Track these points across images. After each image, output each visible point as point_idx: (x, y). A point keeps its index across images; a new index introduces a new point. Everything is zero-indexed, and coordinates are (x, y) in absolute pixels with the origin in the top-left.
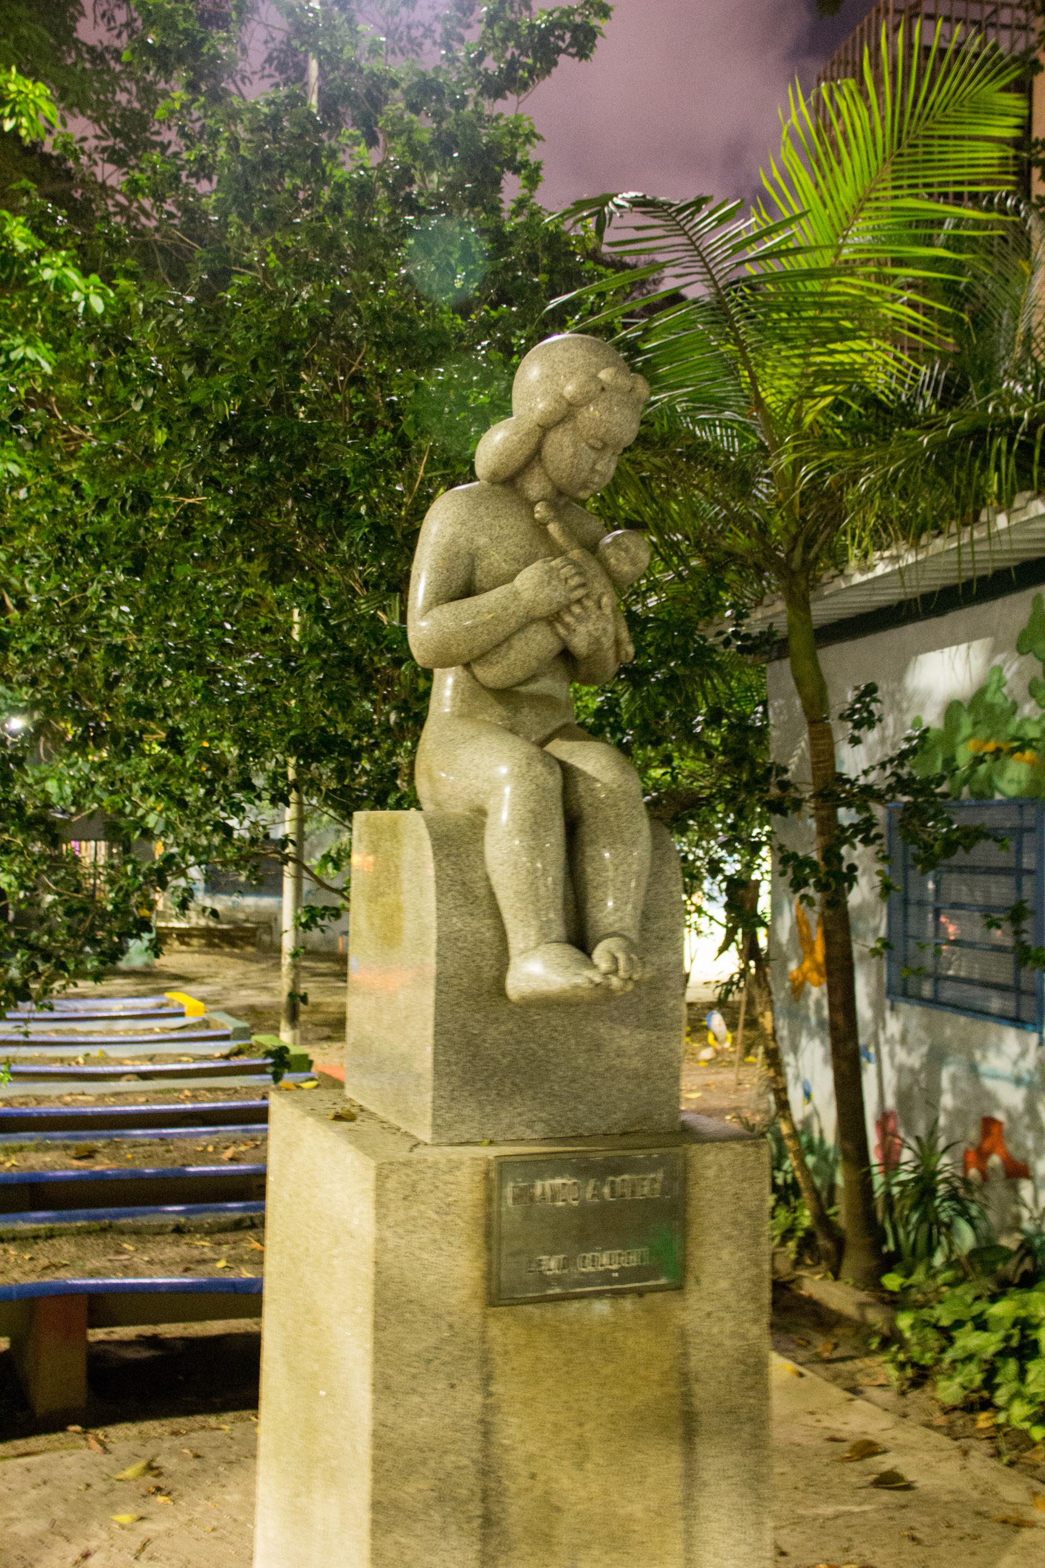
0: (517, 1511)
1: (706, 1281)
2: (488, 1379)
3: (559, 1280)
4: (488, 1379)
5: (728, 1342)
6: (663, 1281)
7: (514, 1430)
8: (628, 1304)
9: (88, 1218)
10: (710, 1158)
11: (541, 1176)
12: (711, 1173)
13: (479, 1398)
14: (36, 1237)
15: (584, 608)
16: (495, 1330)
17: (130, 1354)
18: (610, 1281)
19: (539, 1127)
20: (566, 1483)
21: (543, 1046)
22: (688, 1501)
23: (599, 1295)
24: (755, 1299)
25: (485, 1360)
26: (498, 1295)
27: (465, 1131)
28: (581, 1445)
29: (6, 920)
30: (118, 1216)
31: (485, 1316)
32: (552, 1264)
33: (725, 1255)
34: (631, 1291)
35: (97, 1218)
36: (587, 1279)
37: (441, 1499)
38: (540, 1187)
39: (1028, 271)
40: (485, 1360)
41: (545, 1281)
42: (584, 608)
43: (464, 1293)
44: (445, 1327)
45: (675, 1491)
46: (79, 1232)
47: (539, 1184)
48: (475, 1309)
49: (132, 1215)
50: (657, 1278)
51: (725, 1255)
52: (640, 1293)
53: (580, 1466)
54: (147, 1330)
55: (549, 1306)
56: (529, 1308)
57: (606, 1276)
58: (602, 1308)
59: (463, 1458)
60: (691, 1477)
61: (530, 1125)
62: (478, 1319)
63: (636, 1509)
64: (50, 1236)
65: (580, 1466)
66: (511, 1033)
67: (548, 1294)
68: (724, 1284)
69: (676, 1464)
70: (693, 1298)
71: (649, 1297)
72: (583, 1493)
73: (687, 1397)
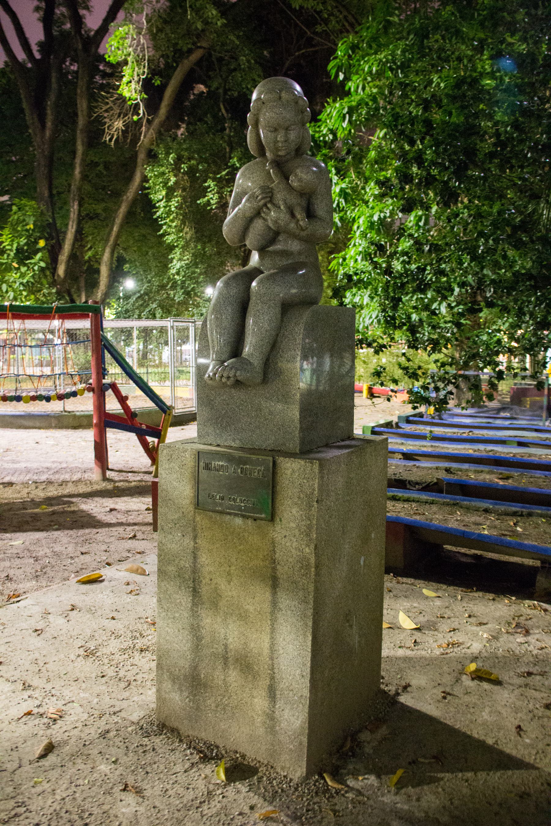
0: (205, 590)
1: (284, 521)
2: (195, 538)
4: (195, 538)
5: (293, 551)
7: (204, 559)
8: (250, 522)
9: (451, 499)
10: (289, 465)
11: (214, 459)
12: (289, 472)
13: (192, 543)
14: (426, 502)
15: (268, 208)
16: (198, 519)
17: (464, 559)
19: (238, 442)
20: (223, 587)
21: (238, 407)
22: (272, 613)
23: (236, 515)
24: (308, 535)
25: (194, 530)
26: (198, 505)
27: (210, 439)
28: (229, 574)
30: (464, 500)
33: (294, 511)
34: (251, 517)
35: (455, 499)
37: (179, 576)
40: (194, 530)
42: (268, 208)
43: (188, 501)
45: (267, 607)
46: (444, 504)
48: (191, 508)
49: (470, 501)
51: (294, 511)
53: (229, 582)
54: (479, 552)
58: (239, 521)
59: (187, 564)
60: (274, 604)
61: (234, 440)
63: (251, 608)
64: (432, 503)
65: (229, 582)
66: (225, 400)
68: (293, 525)
69: (268, 595)
70: (278, 528)
71: (258, 521)
72: (230, 594)
73: (274, 569)
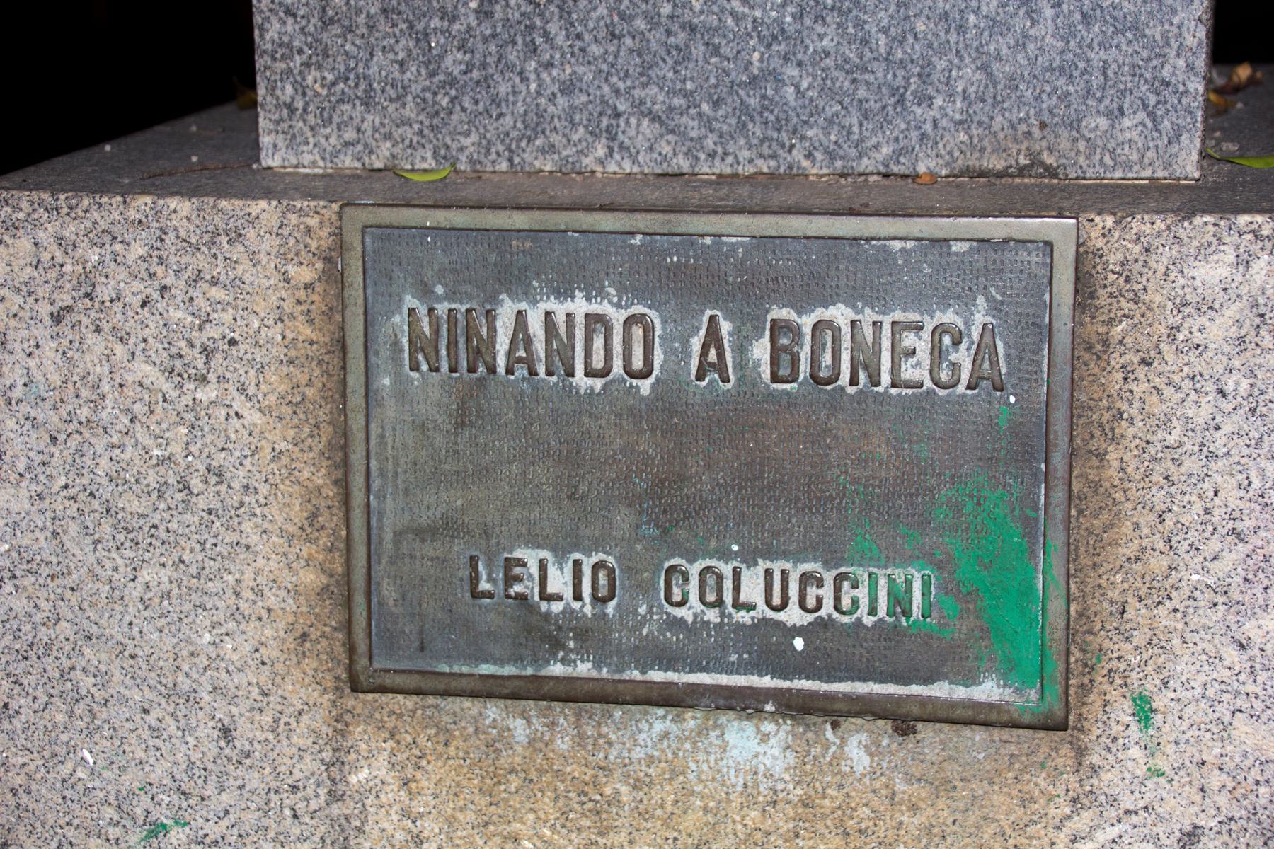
3: (588, 636)
6: (988, 691)
8: (857, 748)
10: (1212, 272)
11: (515, 279)
18: (784, 664)
23: (743, 703)
29: (566, 846)
31: (341, 722)
32: (558, 581)
36: (689, 646)
38: (524, 317)
39: (292, 270)
41: (538, 631)
44: (206, 731)
47: (507, 311)
50: (970, 679)
52: (903, 720)
55: (564, 715)
56: (493, 711)
57: (766, 646)
58: (755, 749)
62: (318, 720)
67: (533, 665)
